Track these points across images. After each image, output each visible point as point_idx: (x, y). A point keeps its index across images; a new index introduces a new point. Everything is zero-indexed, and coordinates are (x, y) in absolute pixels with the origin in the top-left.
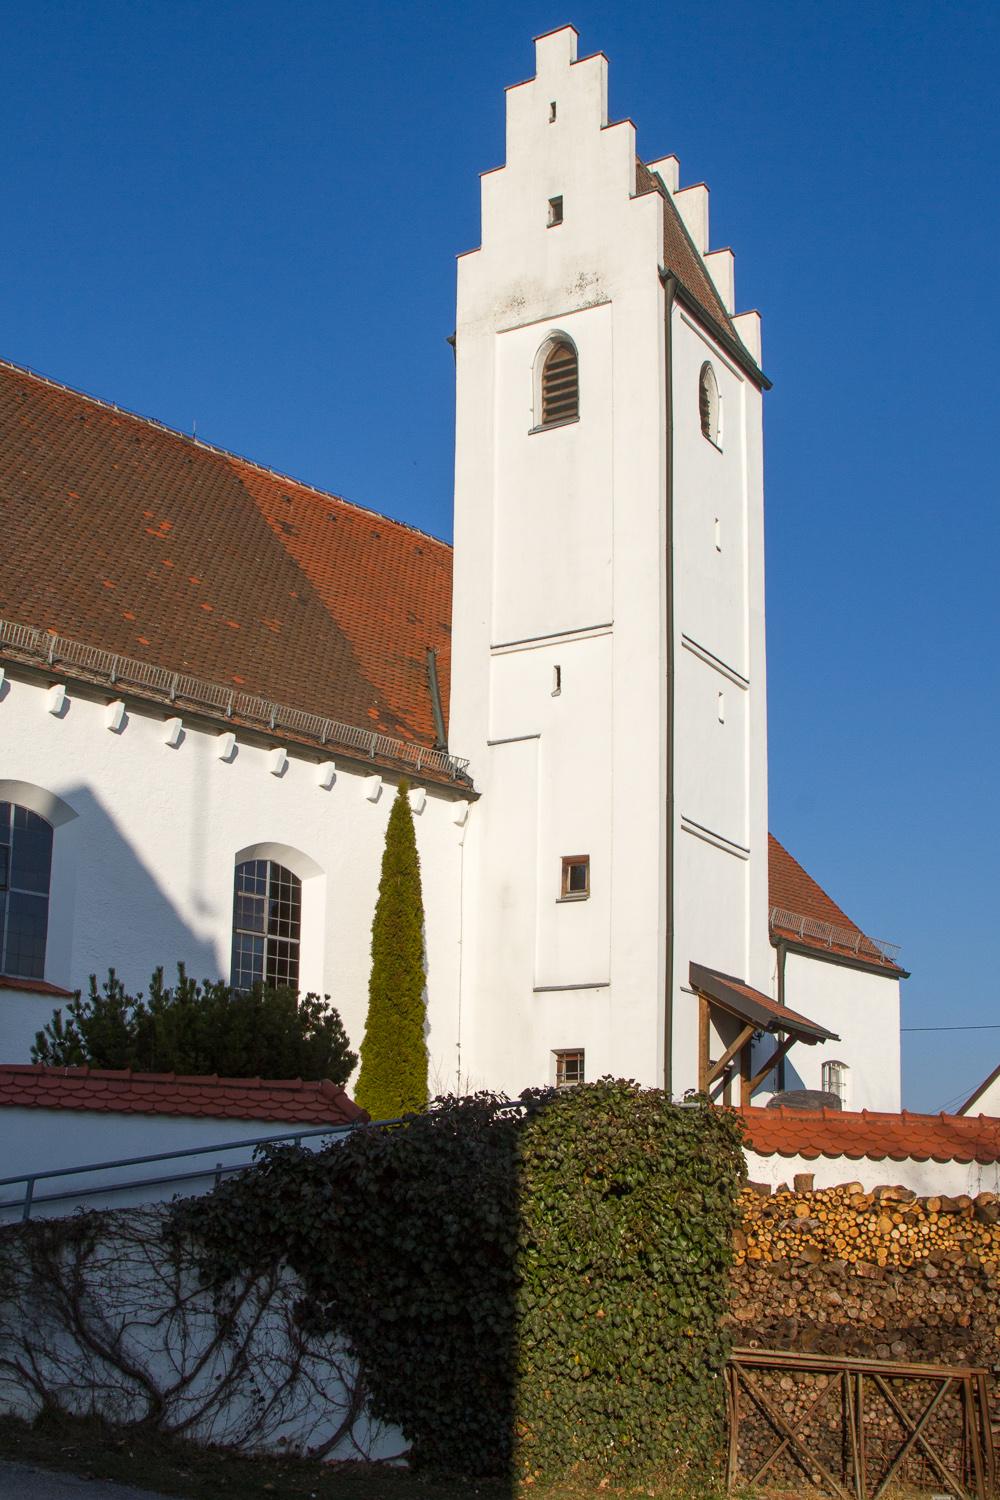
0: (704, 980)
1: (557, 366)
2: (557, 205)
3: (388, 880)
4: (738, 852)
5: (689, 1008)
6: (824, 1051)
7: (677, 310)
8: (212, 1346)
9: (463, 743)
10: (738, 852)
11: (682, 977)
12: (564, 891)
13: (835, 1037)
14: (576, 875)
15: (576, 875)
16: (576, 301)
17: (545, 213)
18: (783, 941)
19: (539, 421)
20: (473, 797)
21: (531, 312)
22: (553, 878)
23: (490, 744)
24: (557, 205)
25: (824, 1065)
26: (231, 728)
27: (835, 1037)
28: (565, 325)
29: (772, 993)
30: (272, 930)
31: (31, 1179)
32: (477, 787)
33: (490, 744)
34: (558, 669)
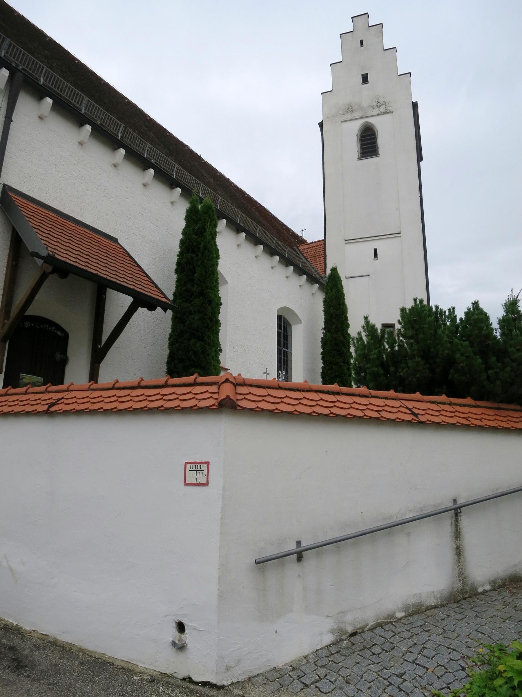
16: (376, 111)
21: (357, 115)
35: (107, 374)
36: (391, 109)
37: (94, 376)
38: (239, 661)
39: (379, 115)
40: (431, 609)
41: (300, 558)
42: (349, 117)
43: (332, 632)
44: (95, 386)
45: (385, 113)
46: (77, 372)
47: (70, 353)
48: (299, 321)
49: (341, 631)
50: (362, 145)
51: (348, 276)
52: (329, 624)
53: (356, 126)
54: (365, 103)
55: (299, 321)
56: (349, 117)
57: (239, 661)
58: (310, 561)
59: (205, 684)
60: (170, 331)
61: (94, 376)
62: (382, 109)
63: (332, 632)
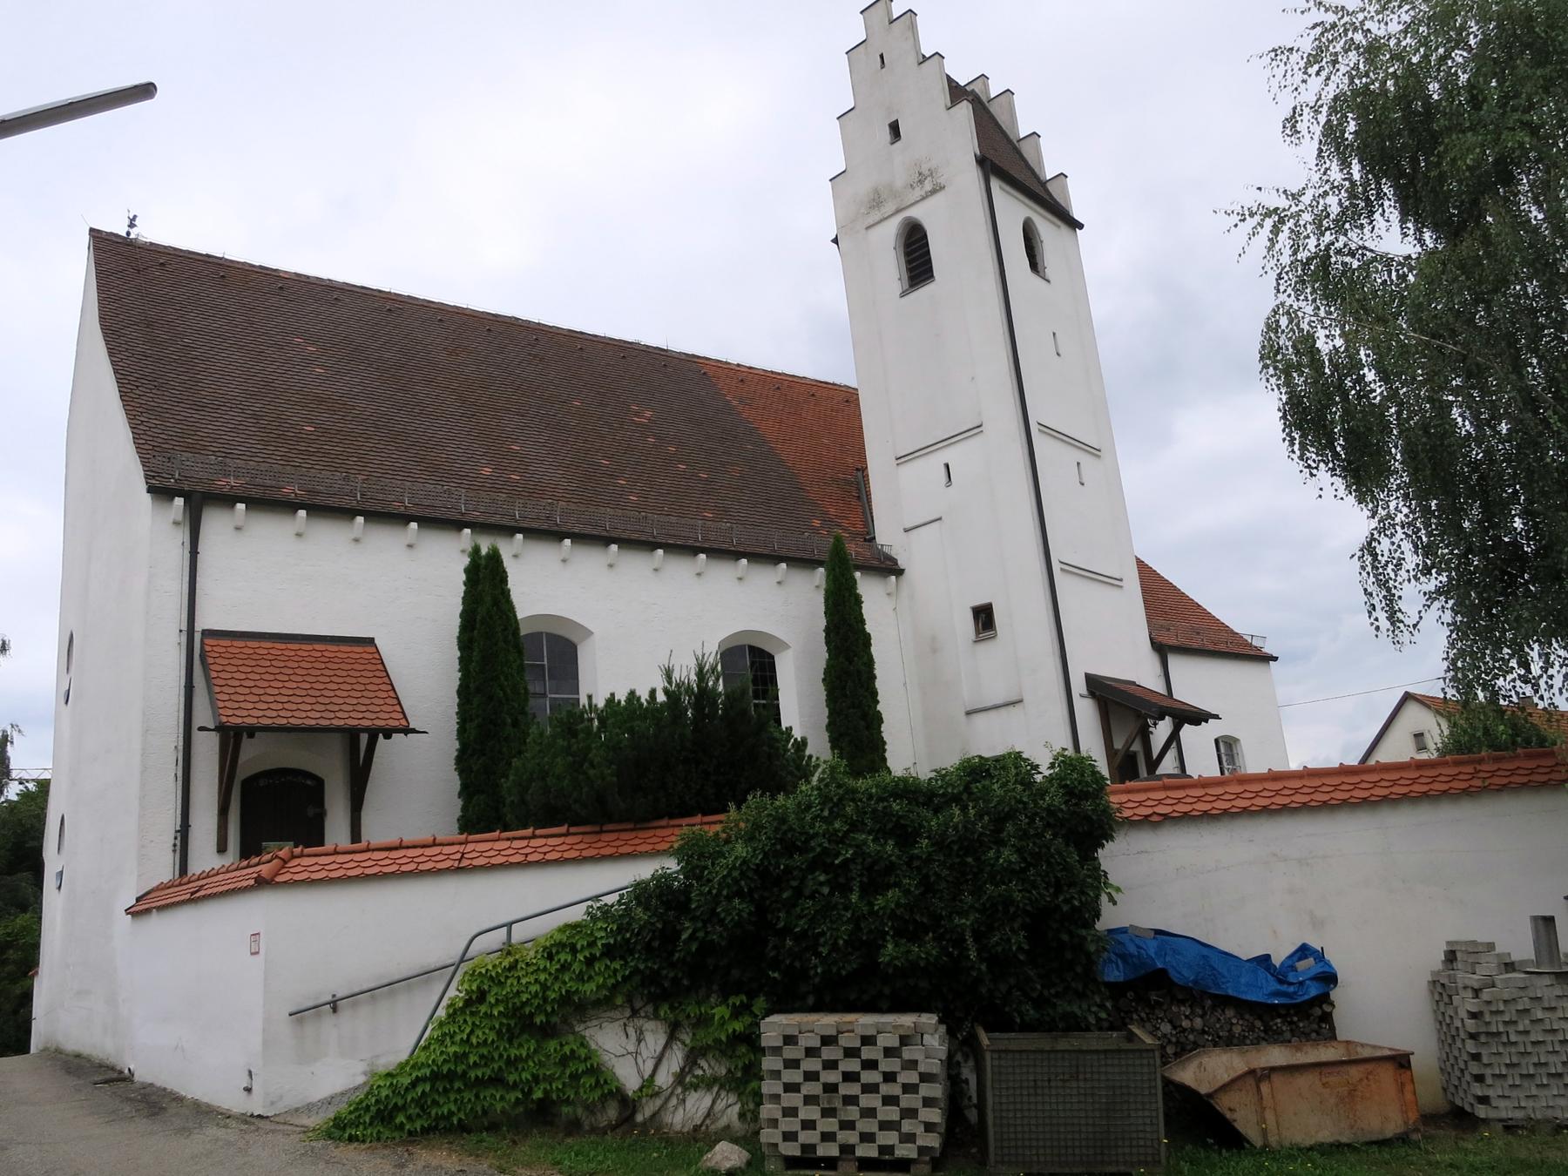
0: (1099, 688)
1: (920, 248)
2: (895, 129)
3: (496, 603)
4: (1114, 582)
5: (1086, 711)
6: (1210, 730)
7: (995, 184)
8: (665, 1048)
9: (886, 534)
10: (1114, 582)
11: (1079, 686)
12: (978, 632)
13: (1216, 717)
14: (984, 617)
15: (984, 617)
16: (918, 193)
17: (886, 134)
18: (1162, 650)
19: (906, 286)
20: (899, 572)
21: (889, 208)
22: (967, 623)
23: (906, 531)
24: (895, 129)
25: (1217, 741)
26: (703, 550)
27: (1216, 717)
28: (916, 213)
29: (1160, 688)
30: (756, 696)
31: (509, 925)
32: (902, 563)
33: (906, 531)
34: (947, 466)
35: (377, 829)
36: (942, 181)
37: (356, 836)
38: (281, 1097)
39: (923, 198)
40: (1291, 1158)
41: (335, 1010)
42: (876, 216)
43: (365, 1074)
44: (356, 846)
45: (933, 192)
46: (337, 830)
47: (327, 806)
48: (784, 646)
49: (374, 1074)
50: (908, 262)
51: (908, 526)
52: (361, 1067)
53: (888, 234)
54: (899, 183)
55: (784, 646)
56: (876, 216)
57: (281, 1097)
58: (345, 1013)
59: (259, 1116)
60: (822, 623)
61: (356, 836)
62: (928, 186)
63: (365, 1074)
